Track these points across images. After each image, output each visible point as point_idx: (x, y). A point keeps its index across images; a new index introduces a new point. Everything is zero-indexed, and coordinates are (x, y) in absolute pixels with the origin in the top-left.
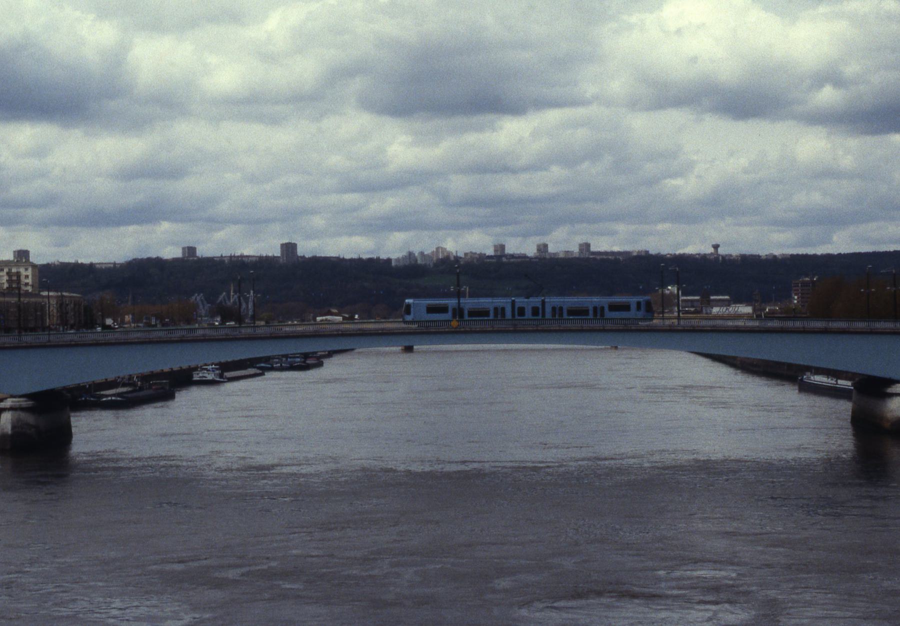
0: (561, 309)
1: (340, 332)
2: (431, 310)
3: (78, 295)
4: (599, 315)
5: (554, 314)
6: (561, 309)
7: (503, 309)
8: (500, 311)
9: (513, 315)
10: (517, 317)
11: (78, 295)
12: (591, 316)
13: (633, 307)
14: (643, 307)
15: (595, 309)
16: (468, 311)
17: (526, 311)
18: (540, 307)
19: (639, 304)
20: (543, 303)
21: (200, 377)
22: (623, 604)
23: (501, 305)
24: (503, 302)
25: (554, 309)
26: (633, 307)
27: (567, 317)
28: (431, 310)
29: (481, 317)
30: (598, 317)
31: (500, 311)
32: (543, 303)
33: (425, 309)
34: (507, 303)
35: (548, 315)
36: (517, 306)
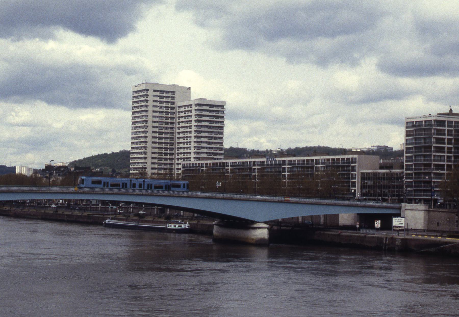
0: (151, 185)
1: (21, 191)
2: (94, 182)
3: (160, 207)
4: (106, 186)
5: (148, 188)
6: (151, 185)
7: (126, 184)
8: (124, 185)
9: (131, 187)
10: (132, 188)
11: (160, 207)
12: (121, 187)
13: (182, 186)
14: (186, 186)
15: (123, 184)
16: (111, 184)
17: (136, 185)
18: (142, 183)
19: (184, 184)
20: (144, 181)
21: (379, 307)
22: (336, 266)
23: (125, 182)
24: (126, 181)
25: (148, 185)
26: (182, 186)
27: (154, 189)
28: (94, 182)
29: (276, 196)
30: (124, 188)
31: (124, 185)
32: (144, 181)
33: (91, 182)
34: (128, 181)
35: (146, 188)
36: (133, 182)
